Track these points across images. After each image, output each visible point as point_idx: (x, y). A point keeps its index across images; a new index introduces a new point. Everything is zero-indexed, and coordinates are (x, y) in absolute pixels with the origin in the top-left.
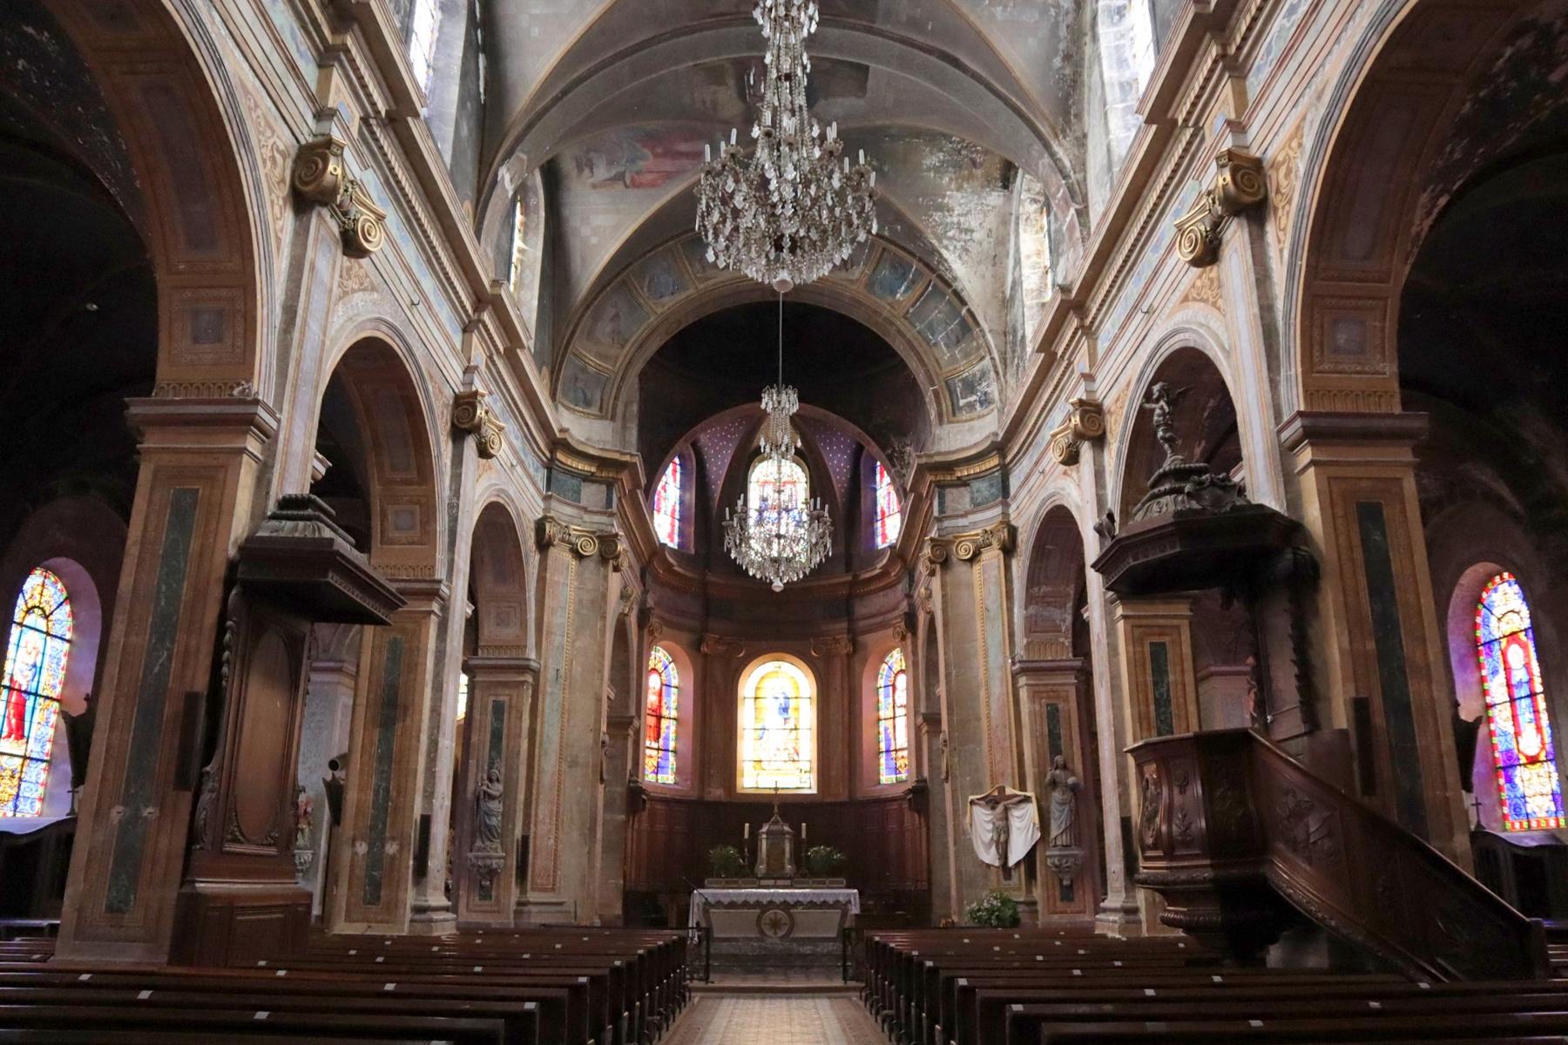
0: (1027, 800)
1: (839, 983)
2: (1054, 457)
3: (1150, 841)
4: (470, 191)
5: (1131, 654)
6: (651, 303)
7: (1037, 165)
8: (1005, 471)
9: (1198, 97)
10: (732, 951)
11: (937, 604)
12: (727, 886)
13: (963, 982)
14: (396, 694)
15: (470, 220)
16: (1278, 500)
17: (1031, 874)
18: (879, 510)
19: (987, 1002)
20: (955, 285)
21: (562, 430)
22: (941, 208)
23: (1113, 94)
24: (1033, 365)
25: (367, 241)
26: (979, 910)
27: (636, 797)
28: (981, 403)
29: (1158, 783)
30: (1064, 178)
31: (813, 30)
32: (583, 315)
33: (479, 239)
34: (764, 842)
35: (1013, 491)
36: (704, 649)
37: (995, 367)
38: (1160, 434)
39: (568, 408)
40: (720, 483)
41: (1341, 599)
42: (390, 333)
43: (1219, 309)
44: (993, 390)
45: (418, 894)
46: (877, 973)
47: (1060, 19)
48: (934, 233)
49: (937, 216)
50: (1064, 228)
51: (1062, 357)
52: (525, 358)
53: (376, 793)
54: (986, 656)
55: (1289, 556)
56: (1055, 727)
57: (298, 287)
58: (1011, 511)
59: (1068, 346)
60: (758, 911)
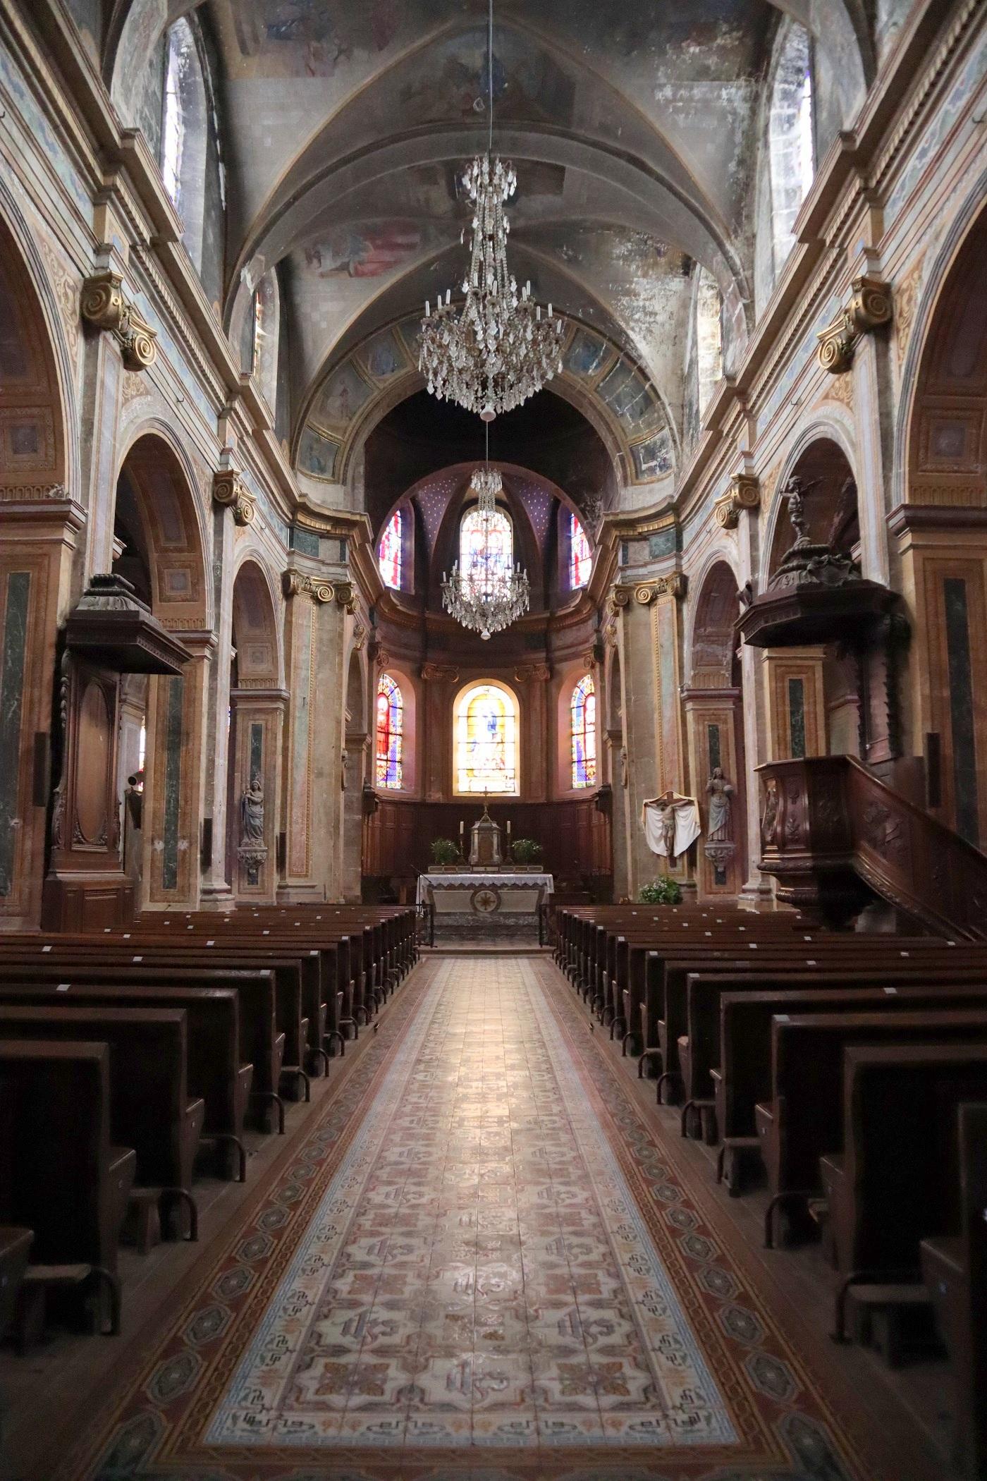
0: (690, 803)
1: (537, 947)
2: (717, 522)
3: (769, 838)
4: (217, 293)
5: (773, 689)
6: (374, 379)
7: (711, 262)
8: (679, 529)
9: (843, 223)
10: (450, 922)
11: (620, 640)
12: (447, 871)
13: (621, 939)
14: (179, 724)
15: (219, 319)
16: (884, 575)
17: (692, 863)
18: (573, 556)
19: (635, 951)
20: (639, 362)
21: (301, 495)
22: (628, 293)
23: (779, 200)
24: (704, 440)
25: (144, 357)
26: (650, 891)
27: (370, 801)
28: (661, 467)
29: (776, 795)
31: (512, 193)
32: (316, 392)
33: (227, 335)
34: (476, 836)
35: (685, 546)
36: (424, 676)
37: (673, 436)
38: (793, 519)
39: (305, 475)
40: (436, 532)
41: (926, 655)
42: (162, 429)
43: (851, 409)
44: (671, 456)
45: (205, 879)
46: (565, 938)
47: (737, 125)
48: (622, 316)
49: (625, 300)
50: (734, 319)
51: (727, 435)
52: (269, 437)
53: (168, 802)
54: (660, 685)
55: (887, 621)
56: (715, 744)
57: (93, 403)
58: (683, 562)
59: (732, 426)
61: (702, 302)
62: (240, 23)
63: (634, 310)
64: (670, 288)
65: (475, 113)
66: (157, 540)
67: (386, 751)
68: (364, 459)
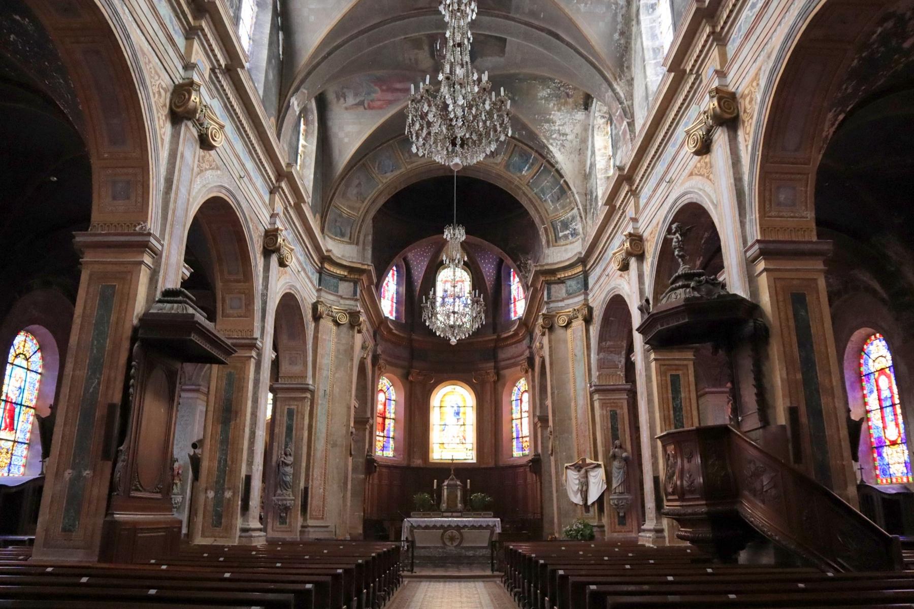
0: (599, 466)
1: (489, 573)
2: (614, 266)
4: (274, 112)
5: (659, 381)
6: (379, 177)
7: (604, 96)
8: (586, 275)
9: (698, 57)
10: (427, 554)
11: (546, 352)
12: (424, 516)
13: (561, 572)
14: (231, 404)
15: (274, 128)
16: (745, 291)
17: (601, 510)
18: (512, 297)
19: (575, 584)
20: (557, 166)
21: (328, 251)
22: (548, 121)
23: (649, 55)
24: (602, 213)
25: (214, 140)
26: (571, 530)
27: (371, 465)
28: (572, 235)
29: (675, 457)
30: (620, 104)
31: (474, 17)
32: (340, 184)
33: (279, 139)
34: (445, 491)
35: (590, 286)
36: (410, 378)
37: (580, 214)
38: (676, 253)
39: (331, 238)
40: (420, 281)
41: (782, 349)
42: (228, 194)
43: (710, 180)
44: (579, 227)
45: (244, 521)
46: (511, 567)
47: (618, 11)
48: (545, 136)
49: (546, 126)
50: (620, 133)
51: (619, 208)
52: (306, 209)
53: (219, 462)
54: (575, 382)
55: (751, 324)
56: (615, 424)
57: (174, 167)
58: (589, 298)
59: (623, 201)
60: (442, 531)
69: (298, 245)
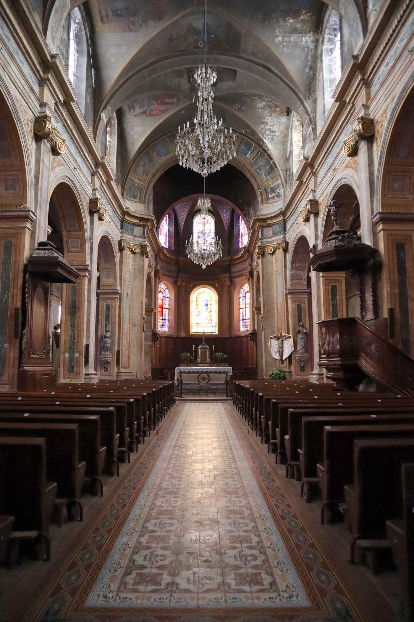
0: (289, 337)
1: (225, 398)
2: (301, 219)
3: (322, 352)
4: (91, 123)
5: (324, 289)
6: (157, 159)
7: (298, 110)
8: (285, 222)
9: (354, 93)
10: (189, 387)
11: (260, 269)
12: (187, 366)
13: (261, 394)
14: (75, 304)
15: (92, 134)
16: (371, 241)
17: (290, 363)
18: (240, 233)
19: (266, 400)
20: (268, 152)
21: (126, 208)
22: (263, 123)
23: (327, 84)
24: (295, 185)
25: (60, 150)
26: (273, 374)
27: (155, 336)
28: (277, 196)
29: (326, 334)
31: (215, 81)
32: (132, 164)
33: (95, 141)
34: (200, 351)
35: (287, 229)
36: (178, 284)
37: (282, 183)
38: (333, 218)
39: (128, 199)
40: (183, 224)
41: (388, 275)
42: (68, 180)
43: (357, 172)
44: (282, 192)
45: (86, 369)
46: (237, 394)
47: (309, 52)
48: (261, 133)
49: (262, 126)
50: (308, 134)
51: (305, 183)
52: (113, 183)
53: (71, 337)
54: (277, 288)
55: (372, 261)
56: (300, 312)
57: (39, 169)
58: (287, 236)
59: (307, 179)
61: (294, 127)
62: (101, 10)
63: (266, 130)
64: (281, 121)
65: (199, 48)
66: (66, 227)
67: (162, 315)
68: (152, 193)
69: (109, 206)
